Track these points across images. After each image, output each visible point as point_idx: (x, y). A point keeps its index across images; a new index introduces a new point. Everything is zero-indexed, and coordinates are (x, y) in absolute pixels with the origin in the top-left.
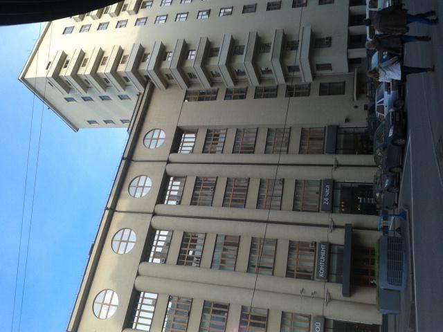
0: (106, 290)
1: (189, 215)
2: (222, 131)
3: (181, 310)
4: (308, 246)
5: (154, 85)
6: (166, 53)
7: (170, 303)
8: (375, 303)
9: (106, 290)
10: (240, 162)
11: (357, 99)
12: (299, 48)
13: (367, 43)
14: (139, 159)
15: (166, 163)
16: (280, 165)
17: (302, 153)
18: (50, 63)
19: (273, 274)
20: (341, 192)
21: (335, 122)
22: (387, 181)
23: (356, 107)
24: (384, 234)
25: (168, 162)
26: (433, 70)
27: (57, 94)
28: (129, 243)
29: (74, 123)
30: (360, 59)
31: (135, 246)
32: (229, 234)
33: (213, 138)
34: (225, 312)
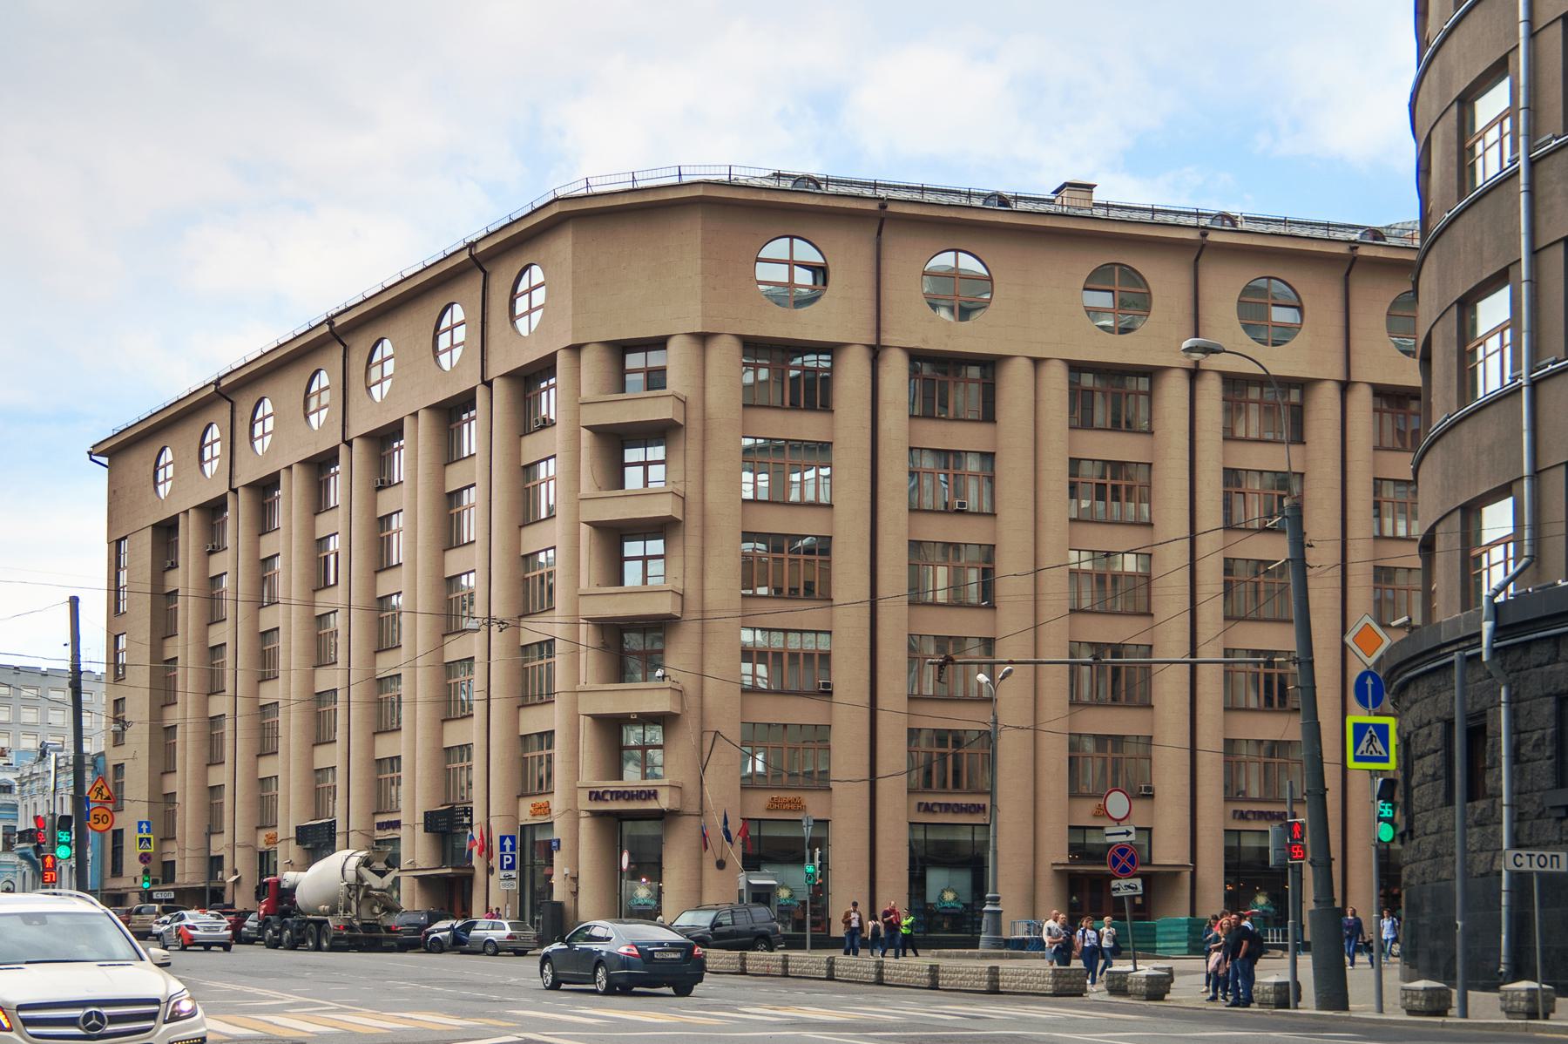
0: (1300, 308)
1: (1339, 345)
2: (1145, 506)
3: (802, 567)
4: (956, 496)
5: (1244, 290)
6: (1413, 815)
7: (762, 441)
8: (1273, 308)
9: (1300, 308)
10: (1199, 435)
11: (1055, 871)
12: (340, 735)
13: (1251, 928)
14: (67, 653)
15: (1342, 377)
16: (1035, 725)
17: (909, 545)
18: (74, 602)
19: (1071, 520)
20: (807, 354)
21: (1383, 321)
22: (1503, 690)
23: (135, 879)
24: (1379, 840)
25: (1345, 386)
26: (830, 632)
27: (1296, 699)
28: (1032, 569)
29: (874, 276)
30: (552, 866)
31: (1462, 513)
32: (997, 552)
33: (1109, 481)
34: (1404, 445)
